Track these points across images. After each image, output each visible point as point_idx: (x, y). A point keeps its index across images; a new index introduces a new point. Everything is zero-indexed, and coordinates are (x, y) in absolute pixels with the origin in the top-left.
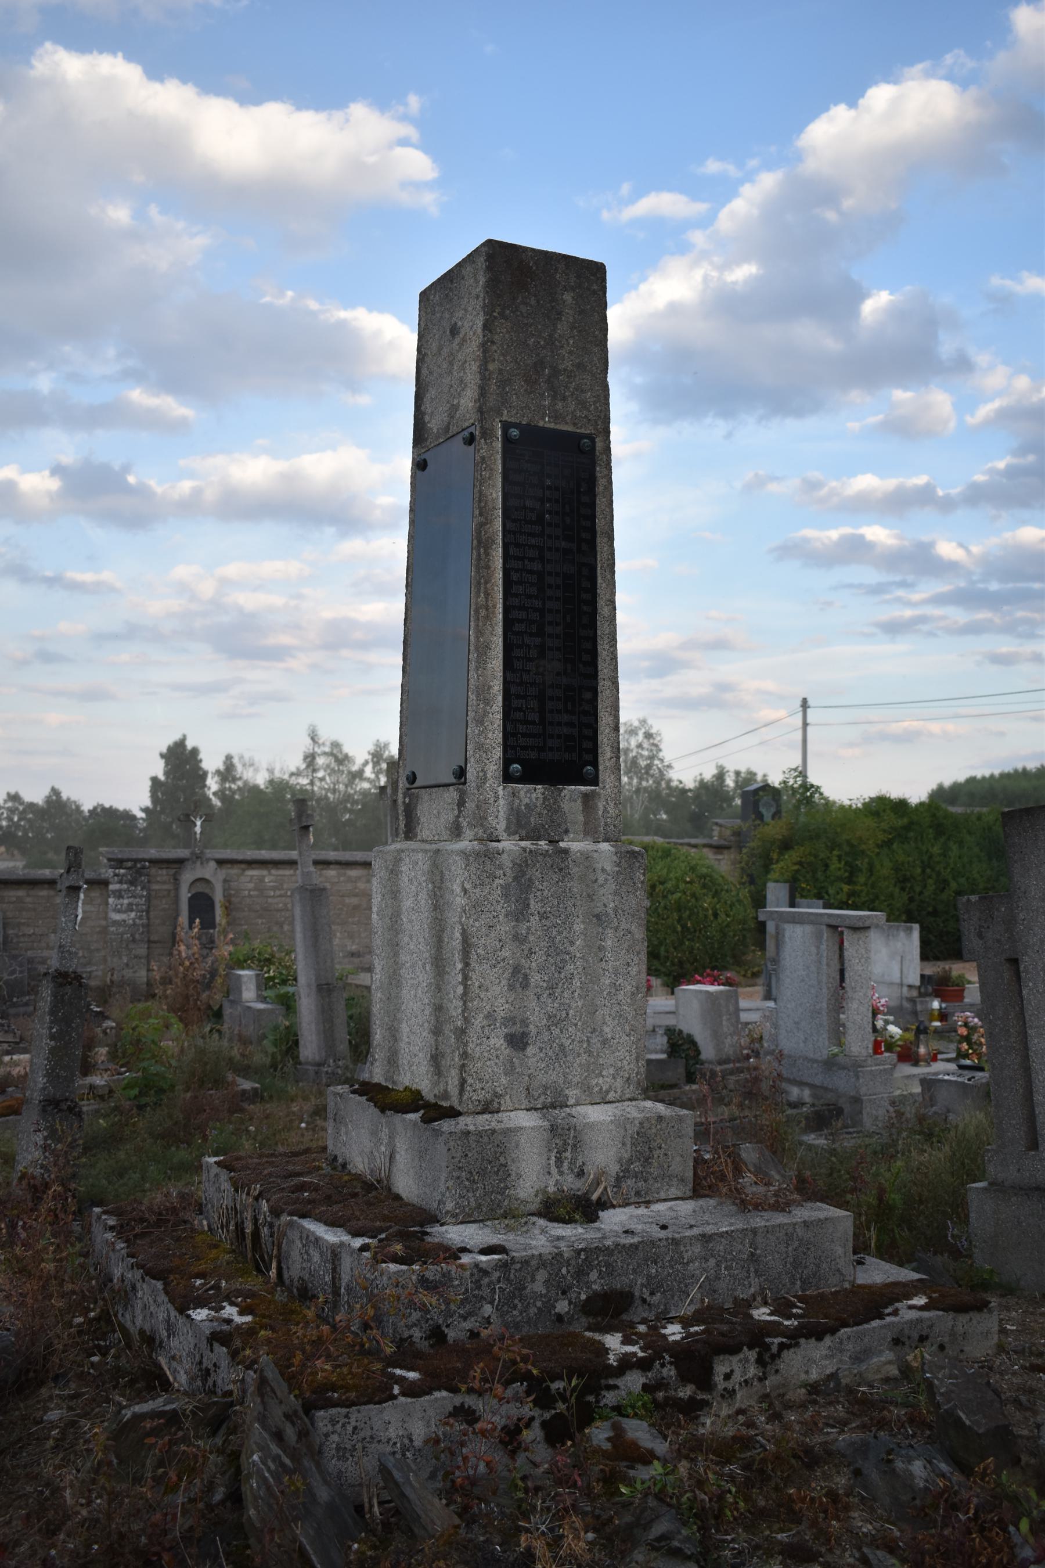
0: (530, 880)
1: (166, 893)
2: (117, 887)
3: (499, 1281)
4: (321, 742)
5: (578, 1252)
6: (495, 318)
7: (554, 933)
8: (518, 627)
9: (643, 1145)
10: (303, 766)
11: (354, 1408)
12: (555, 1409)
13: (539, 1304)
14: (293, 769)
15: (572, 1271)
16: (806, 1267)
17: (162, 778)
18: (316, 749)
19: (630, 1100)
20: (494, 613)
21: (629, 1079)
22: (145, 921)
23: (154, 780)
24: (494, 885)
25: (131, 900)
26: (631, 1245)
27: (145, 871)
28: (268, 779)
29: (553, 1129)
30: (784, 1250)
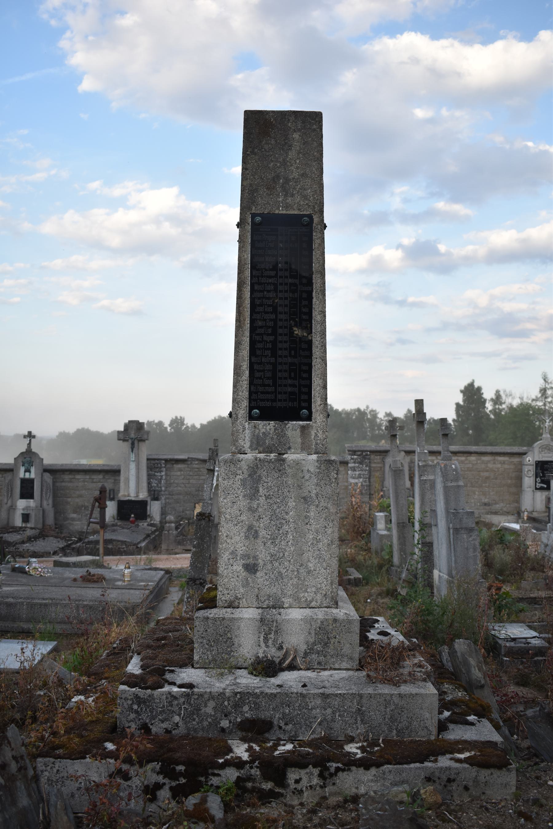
0: (259, 476)
1: (379, 469)
2: (353, 465)
3: (184, 704)
4: (549, 381)
5: (236, 694)
6: (248, 155)
7: (275, 507)
8: (259, 331)
9: (324, 636)
10: (539, 395)
11: (59, 760)
12: (179, 781)
13: (210, 720)
14: (534, 397)
15: (231, 704)
16: (400, 722)
17: (461, 403)
18: (547, 386)
19: (326, 607)
20: (244, 324)
21: (325, 595)
22: (368, 483)
23: (458, 404)
24: (236, 479)
25: (360, 472)
26: (272, 694)
27: (368, 457)
28: (520, 403)
29: (262, 620)
30: (383, 710)
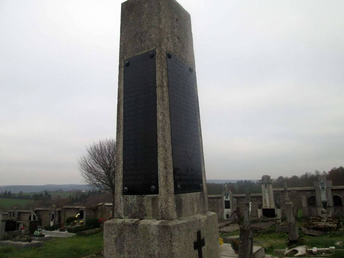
0: (124, 236)
